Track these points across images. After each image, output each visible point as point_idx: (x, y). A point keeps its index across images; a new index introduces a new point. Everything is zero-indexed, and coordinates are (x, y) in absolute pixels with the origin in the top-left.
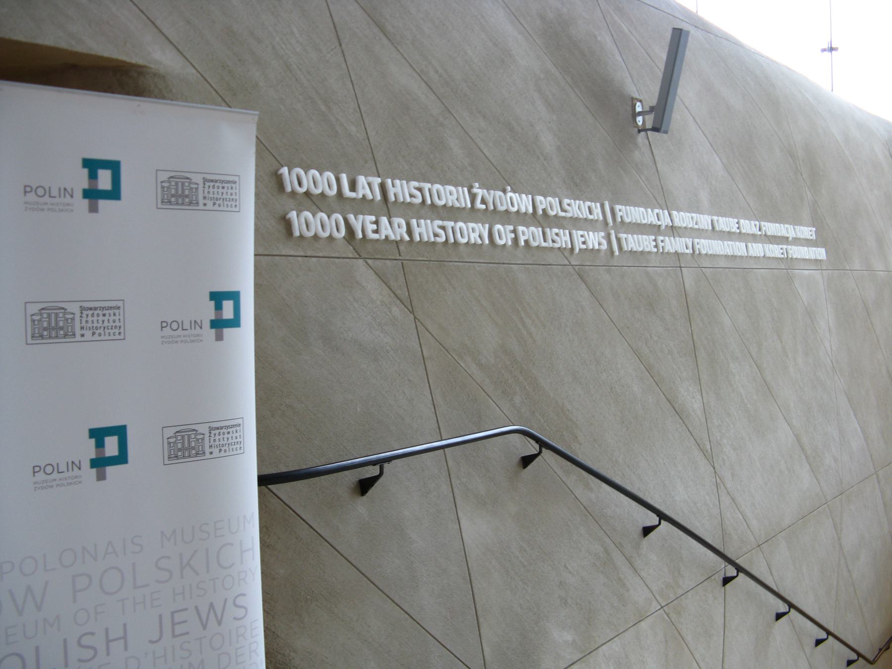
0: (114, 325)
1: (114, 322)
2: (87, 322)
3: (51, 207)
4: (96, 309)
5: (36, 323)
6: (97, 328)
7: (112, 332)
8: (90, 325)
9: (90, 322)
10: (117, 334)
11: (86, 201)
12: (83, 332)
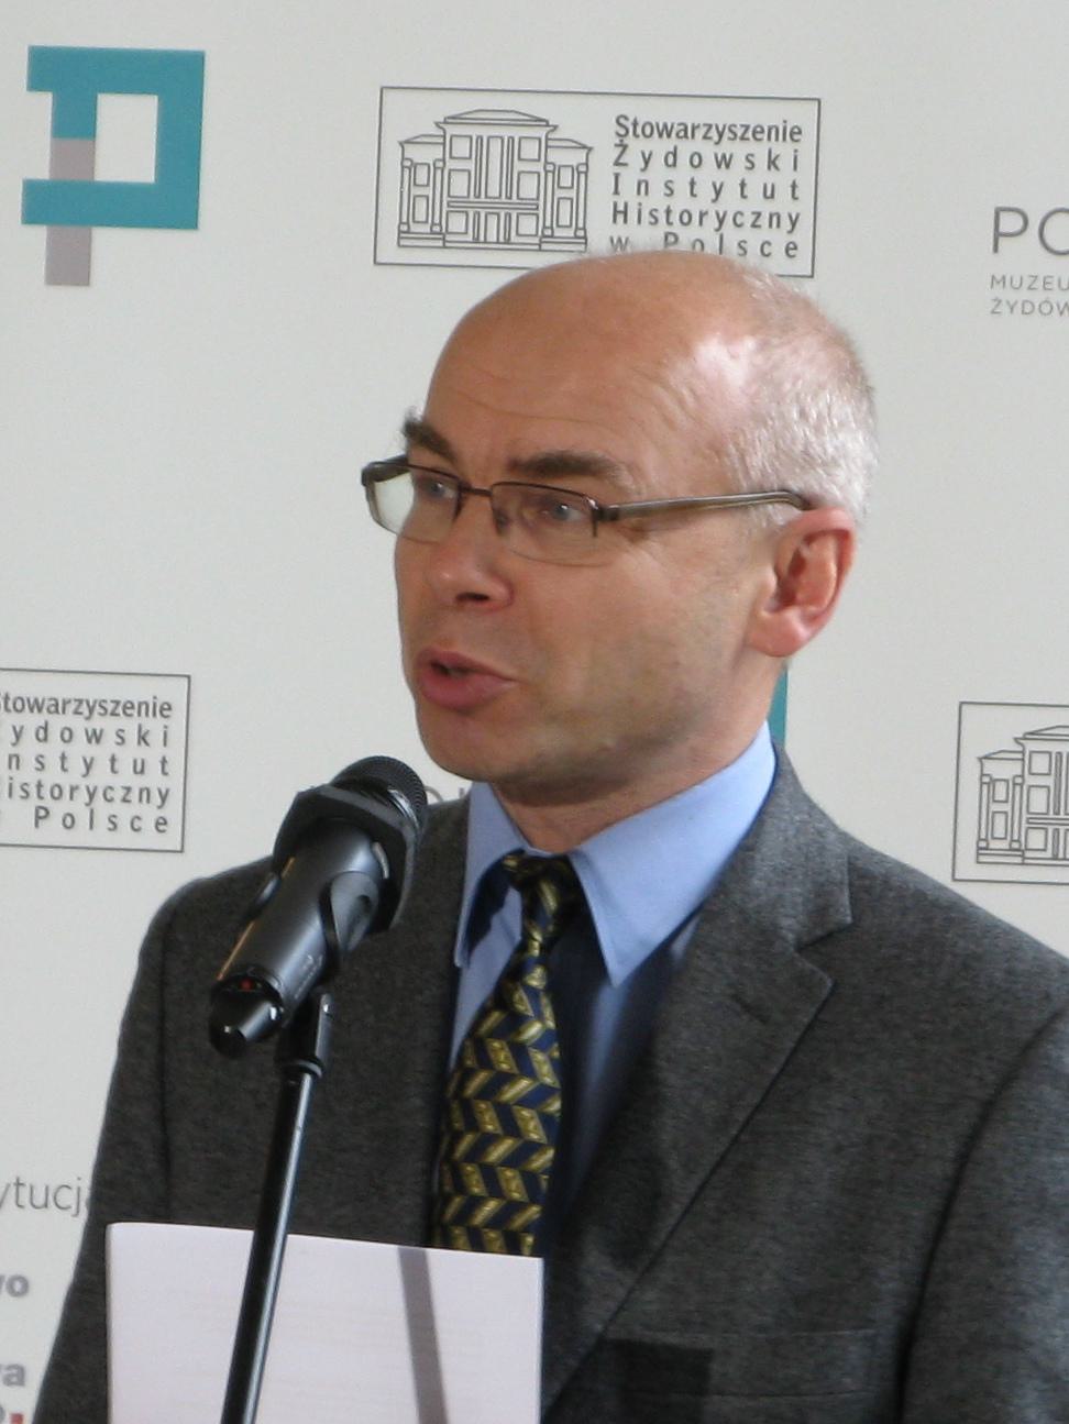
0: (137, 782)
1: (769, 194)
2: (643, 187)
4: (57, 707)
5: (422, 176)
6: (57, 792)
7: (125, 813)
8: (656, 199)
9: (657, 189)
10: (148, 824)
11: (39, 235)
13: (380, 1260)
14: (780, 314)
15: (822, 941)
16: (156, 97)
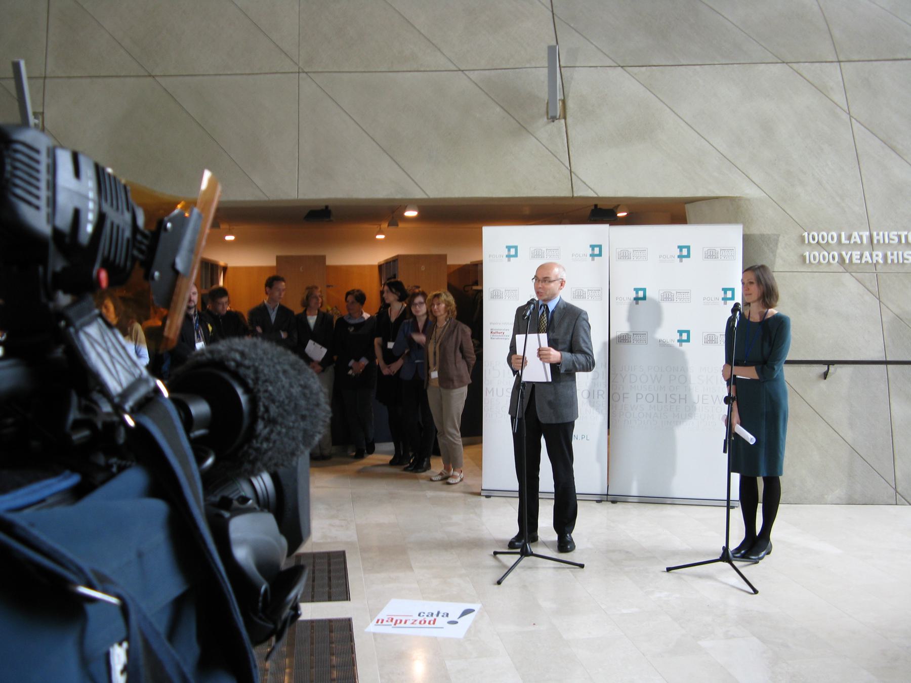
13: (536, 335)
14: (559, 266)
15: (564, 308)
16: (577, 373)
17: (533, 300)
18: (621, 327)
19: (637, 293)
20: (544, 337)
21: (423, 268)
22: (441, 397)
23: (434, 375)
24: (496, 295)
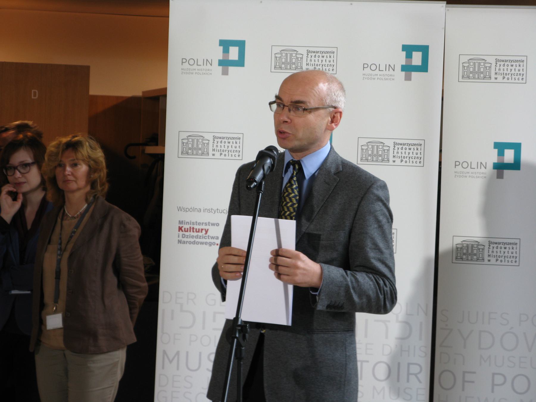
3: (471, 175)
6: (499, 257)
8: (400, 155)
12: (489, 258)
14: (331, 80)
15: (337, 173)
17: (271, 149)
18: (467, 225)
19: (501, 154)
20: (289, 227)
21: (35, 94)
22: (66, 371)
23: (54, 321)
24: (194, 147)
